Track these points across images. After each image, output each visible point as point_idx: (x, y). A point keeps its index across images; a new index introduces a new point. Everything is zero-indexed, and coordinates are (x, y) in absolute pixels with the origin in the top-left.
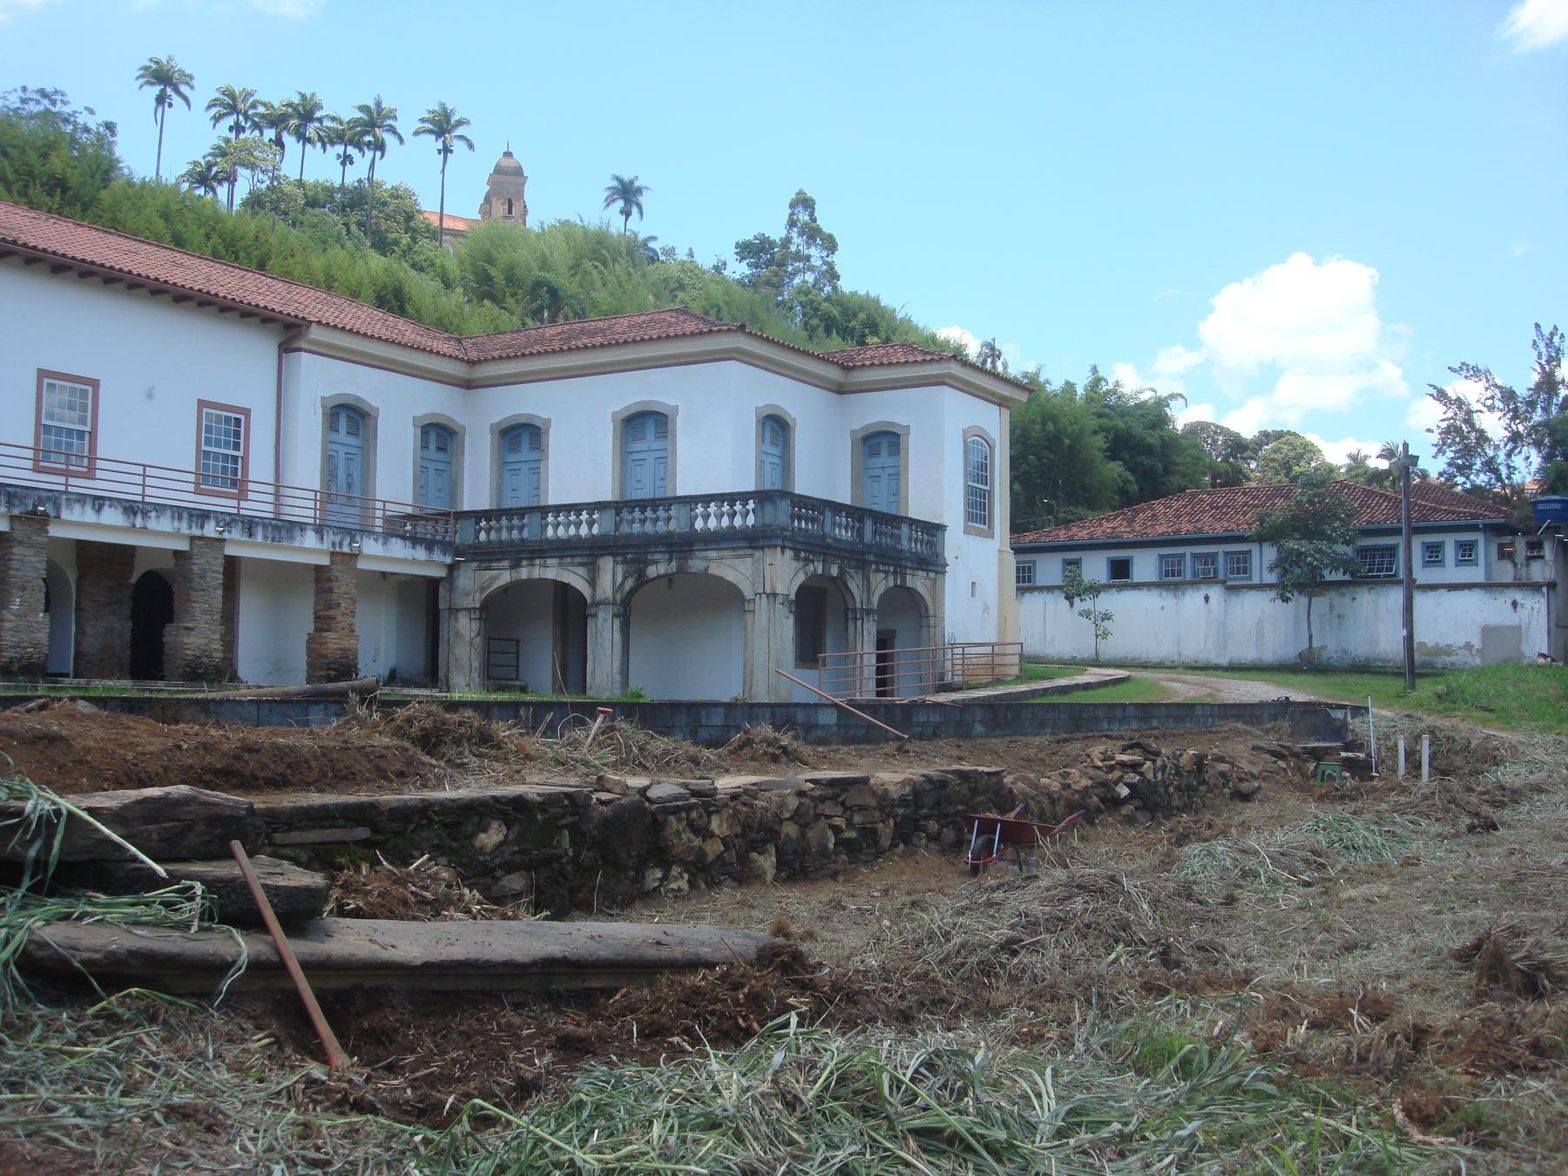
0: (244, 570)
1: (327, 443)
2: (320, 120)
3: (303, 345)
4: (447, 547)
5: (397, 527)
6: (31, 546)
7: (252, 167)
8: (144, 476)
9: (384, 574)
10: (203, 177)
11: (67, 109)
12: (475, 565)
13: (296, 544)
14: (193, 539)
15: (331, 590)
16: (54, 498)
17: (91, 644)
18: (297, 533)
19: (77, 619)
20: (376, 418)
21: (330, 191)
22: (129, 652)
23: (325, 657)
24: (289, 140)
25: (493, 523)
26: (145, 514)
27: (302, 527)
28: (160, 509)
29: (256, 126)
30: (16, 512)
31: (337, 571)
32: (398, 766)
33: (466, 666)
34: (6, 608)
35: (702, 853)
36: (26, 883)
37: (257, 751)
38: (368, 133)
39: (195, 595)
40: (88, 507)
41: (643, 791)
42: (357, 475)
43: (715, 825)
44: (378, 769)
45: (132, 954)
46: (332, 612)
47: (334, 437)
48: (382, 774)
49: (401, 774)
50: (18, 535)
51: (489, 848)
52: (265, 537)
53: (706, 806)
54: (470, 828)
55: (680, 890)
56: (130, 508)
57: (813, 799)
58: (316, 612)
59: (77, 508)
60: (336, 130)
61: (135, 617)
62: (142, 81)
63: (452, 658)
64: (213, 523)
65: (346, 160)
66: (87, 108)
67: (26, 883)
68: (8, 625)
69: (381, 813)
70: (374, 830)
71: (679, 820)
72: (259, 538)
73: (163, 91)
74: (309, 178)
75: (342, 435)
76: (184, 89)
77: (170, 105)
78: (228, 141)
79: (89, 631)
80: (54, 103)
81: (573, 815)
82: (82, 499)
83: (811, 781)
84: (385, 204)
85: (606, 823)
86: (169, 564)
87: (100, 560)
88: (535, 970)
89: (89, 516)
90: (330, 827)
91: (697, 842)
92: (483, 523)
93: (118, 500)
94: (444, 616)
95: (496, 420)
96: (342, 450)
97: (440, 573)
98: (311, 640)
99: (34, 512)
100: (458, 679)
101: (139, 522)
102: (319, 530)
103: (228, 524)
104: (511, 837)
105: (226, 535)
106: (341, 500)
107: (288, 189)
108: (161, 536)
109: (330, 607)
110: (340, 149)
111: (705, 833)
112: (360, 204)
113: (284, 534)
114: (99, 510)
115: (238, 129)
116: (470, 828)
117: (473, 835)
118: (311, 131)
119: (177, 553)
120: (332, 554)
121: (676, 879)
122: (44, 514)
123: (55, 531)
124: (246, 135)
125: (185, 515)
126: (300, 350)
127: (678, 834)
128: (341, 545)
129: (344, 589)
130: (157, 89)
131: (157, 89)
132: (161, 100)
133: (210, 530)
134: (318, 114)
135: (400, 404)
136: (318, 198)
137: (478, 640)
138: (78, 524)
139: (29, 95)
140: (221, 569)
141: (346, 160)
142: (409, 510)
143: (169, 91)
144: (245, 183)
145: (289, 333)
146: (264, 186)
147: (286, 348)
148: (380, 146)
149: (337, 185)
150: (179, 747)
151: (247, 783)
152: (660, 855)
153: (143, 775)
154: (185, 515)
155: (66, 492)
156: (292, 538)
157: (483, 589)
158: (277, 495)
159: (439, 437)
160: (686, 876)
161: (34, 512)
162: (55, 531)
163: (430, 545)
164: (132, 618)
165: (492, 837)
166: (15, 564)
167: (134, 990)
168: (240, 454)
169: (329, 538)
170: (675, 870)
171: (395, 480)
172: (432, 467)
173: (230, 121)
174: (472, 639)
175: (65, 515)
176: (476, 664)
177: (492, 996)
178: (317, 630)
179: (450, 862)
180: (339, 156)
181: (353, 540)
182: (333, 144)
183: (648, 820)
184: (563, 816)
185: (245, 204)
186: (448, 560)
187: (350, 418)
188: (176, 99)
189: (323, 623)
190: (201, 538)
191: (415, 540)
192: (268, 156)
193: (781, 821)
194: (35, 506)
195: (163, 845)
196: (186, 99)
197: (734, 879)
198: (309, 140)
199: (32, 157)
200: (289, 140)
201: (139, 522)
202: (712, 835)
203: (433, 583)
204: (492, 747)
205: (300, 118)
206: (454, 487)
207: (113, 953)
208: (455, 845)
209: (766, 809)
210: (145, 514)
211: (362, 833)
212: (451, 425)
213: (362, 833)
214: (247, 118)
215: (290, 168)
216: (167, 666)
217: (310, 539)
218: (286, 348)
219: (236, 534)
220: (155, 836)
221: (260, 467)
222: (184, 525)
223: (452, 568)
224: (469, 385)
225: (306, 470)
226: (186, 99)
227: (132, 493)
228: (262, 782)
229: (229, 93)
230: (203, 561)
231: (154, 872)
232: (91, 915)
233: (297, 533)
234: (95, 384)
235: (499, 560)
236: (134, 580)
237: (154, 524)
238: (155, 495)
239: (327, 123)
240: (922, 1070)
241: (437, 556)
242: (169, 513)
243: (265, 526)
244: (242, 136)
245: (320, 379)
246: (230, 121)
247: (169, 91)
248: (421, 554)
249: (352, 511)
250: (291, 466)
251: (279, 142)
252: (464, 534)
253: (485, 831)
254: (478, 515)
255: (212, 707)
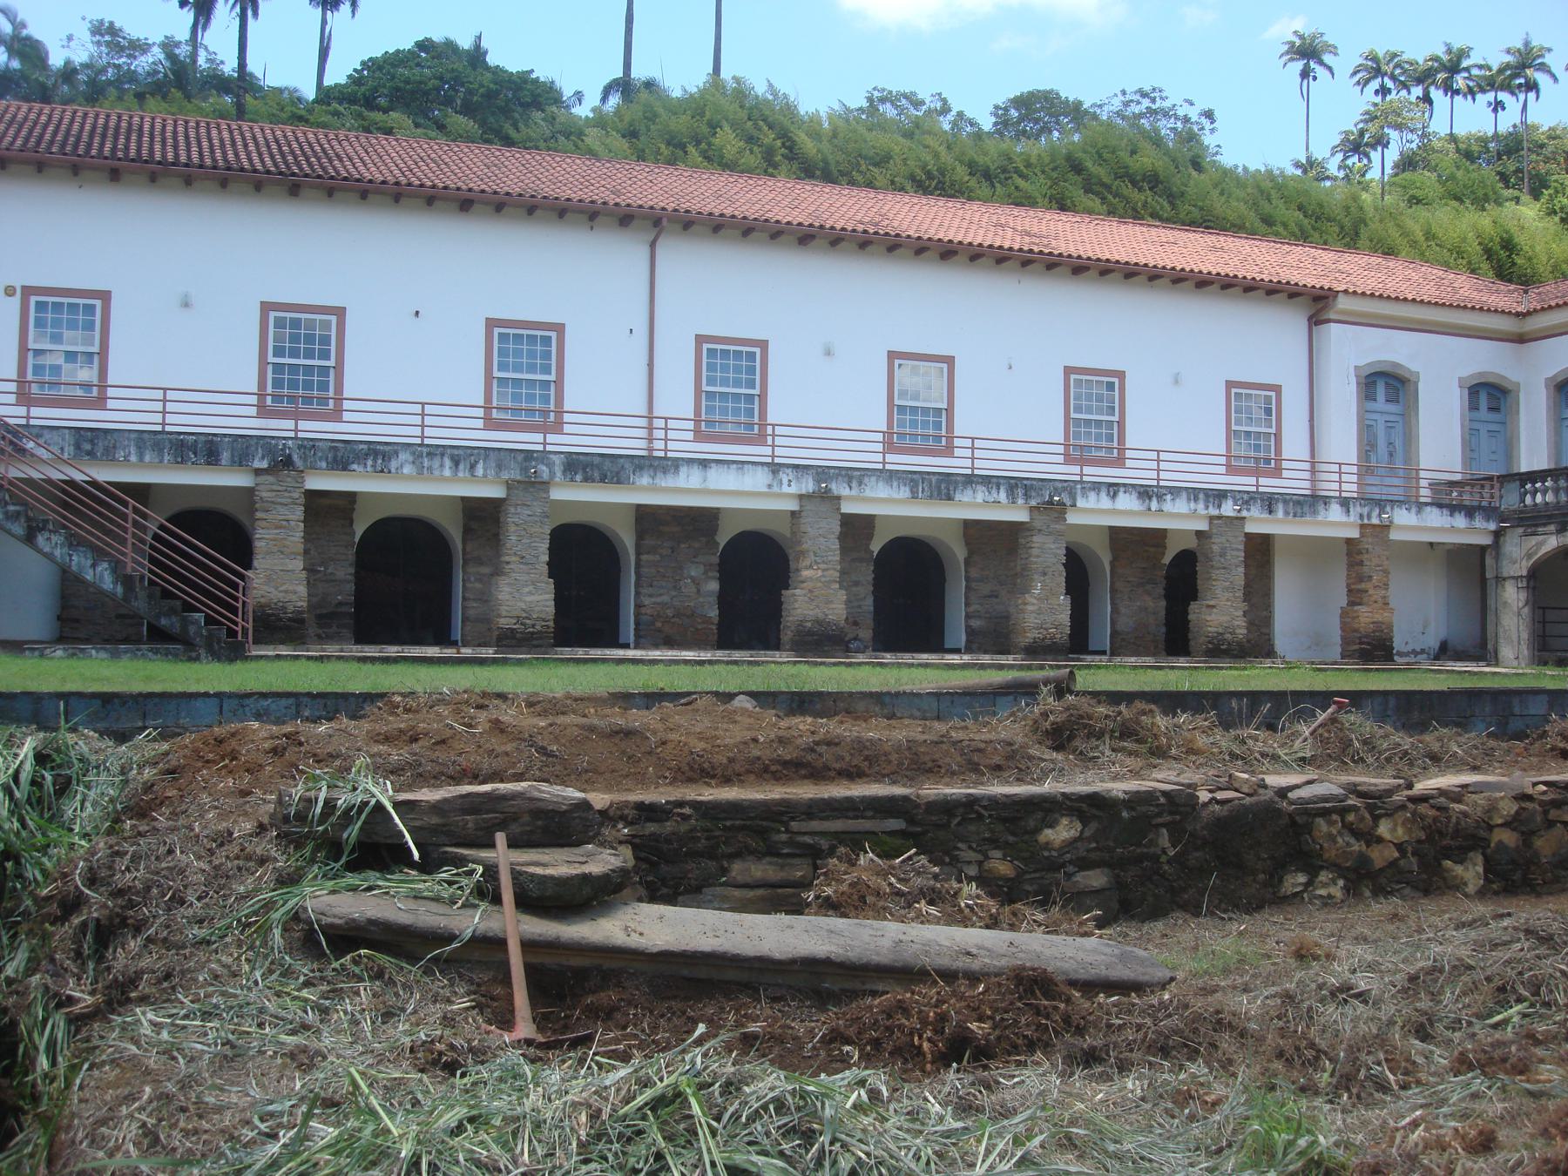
0: (1278, 548)
1: (1362, 414)
2: (1467, 69)
3: (1332, 316)
4: (1490, 512)
5: (1448, 497)
6: (1050, 533)
7: (1399, 127)
8: (1158, 461)
9: (1431, 544)
10: (1355, 145)
11: (1167, 104)
12: (1521, 530)
13: (1320, 518)
14: (1211, 518)
15: (1361, 563)
16: (1069, 487)
17: (1126, 623)
18: (1321, 507)
19: (1112, 599)
20: (1416, 384)
21: (1483, 141)
22: (1163, 630)
23: (1356, 631)
24: (1436, 94)
25: (1538, 485)
26: (1160, 498)
27: (1326, 501)
28: (1175, 491)
29: (1405, 86)
30: (1033, 503)
31: (1367, 544)
32: (997, 760)
33: (1515, 638)
34: (1028, 592)
35: (1364, 860)
36: (343, 860)
37: (837, 744)
38: (1517, 76)
39: (1215, 574)
40: (1103, 494)
41: (1282, 792)
42: (1398, 443)
43: (1384, 829)
44: (970, 762)
45: (371, 922)
46: (1363, 586)
47: (1371, 405)
48: (975, 768)
49: (998, 768)
50: (1037, 524)
51: (1057, 844)
52: (1286, 513)
53: (1371, 808)
54: (1032, 823)
55: (1330, 896)
56: (1145, 493)
57: (1542, 804)
58: (1348, 585)
59: (1092, 495)
60: (1484, 77)
61: (1168, 596)
62: (1286, 58)
63: (1501, 630)
64: (1230, 502)
65: (1498, 106)
66: (1186, 101)
67: (343, 860)
68: (1030, 608)
69: (918, 806)
70: (911, 821)
71: (1331, 823)
72: (1280, 514)
73: (1307, 66)
74: (1461, 131)
75: (1381, 403)
76: (1327, 58)
77: (1315, 78)
78: (1375, 105)
79: (1123, 610)
80: (1153, 101)
81: (1171, 813)
82: (1096, 487)
83: (1545, 783)
84: (1542, 146)
85: (1220, 824)
86: (1192, 544)
87: (1133, 545)
88: (796, 967)
89: (1105, 502)
90: (856, 818)
91: (1357, 846)
92: (1528, 486)
93: (1133, 486)
94: (1491, 584)
95: (1551, 374)
96: (1381, 419)
97: (1486, 540)
98: (1344, 614)
99: (1051, 502)
100: (1506, 652)
101: (1154, 505)
102: (1345, 503)
103: (1247, 502)
104: (1087, 834)
105: (1244, 513)
106: (1381, 472)
107: (1436, 144)
108: (1180, 519)
109: (1361, 579)
110: (1490, 96)
111: (1372, 839)
112: (1518, 150)
113: (1306, 509)
114: (1114, 497)
115: (1383, 91)
116: (1032, 823)
117: (1038, 830)
118: (1460, 81)
119: (1199, 533)
120: (1362, 526)
121: (1325, 885)
122: (1061, 503)
123: (1072, 518)
124: (1392, 96)
125: (1201, 496)
126: (1329, 321)
127: (1332, 838)
128: (1369, 517)
129: (1375, 561)
130: (1300, 65)
131: (1300, 65)
132: (1305, 74)
133: (1228, 509)
134: (1465, 64)
135: (1442, 369)
136: (1468, 151)
137: (1526, 610)
138: (1094, 513)
139: (1128, 97)
140: (1242, 547)
141: (1498, 106)
142: (1458, 477)
143: (1312, 64)
144: (1398, 145)
145: (1317, 305)
146: (1414, 146)
147: (1316, 321)
148: (1532, 86)
149: (1490, 134)
150: (755, 740)
151: (817, 774)
152: (1311, 862)
153: (706, 765)
154: (1201, 496)
155: (1081, 482)
156: (1315, 513)
157: (1529, 556)
158: (1313, 471)
159: (1489, 397)
160: (1341, 883)
161: (1051, 502)
162: (1072, 518)
163: (1470, 512)
164: (1167, 597)
165: (1062, 832)
166: (1035, 552)
167: (362, 952)
168: (332, 363)
169: (1356, 510)
170: (1324, 876)
171: (1440, 445)
172: (1484, 428)
173: (1375, 84)
174: (1519, 610)
175: (1081, 503)
176: (1525, 635)
177: (751, 989)
178: (1351, 603)
179: (1005, 856)
180: (1490, 104)
181: (1382, 511)
182: (1483, 91)
183: (1286, 820)
184: (1159, 815)
185: (1396, 166)
186: (1492, 526)
187: (1387, 386)
188: (1320, 71)
189: (1355, 597)
190: (1220, 517)
191: (1453, 509)
192: (1415, 116)
193: (1491, 828)
194: (1051, 497)
195: (480, 833)
196: (1330, 69)
197: (1416, 888)
198: (1457, 92)
199: (1124, 155)
200: (1436, 94)
201: (1154, 505)
202: (1380, 840)
203: (1483, 549)
204: (1137, 741)
205: (1447, 72)
206: (1509, 449)
207: (354, 920)
208: (1011, 839)
209: (1465, 815)
210: (1160, 498)
211: (895, 824)
212: (1504, 384)
213: (895, 824)
214: (1393, 78)
215: (1439, 125)
216: (1192, 643)
217: (1335, 513)
218: (1316, 321)
219: (1255, 512)
220: (470, 825)
221: (1294, 445)
222: (1201, 506)
223: (1498, 534)
224: (1521, 339)
225: (1342, 444)
226: (1330, 69)
227: (1147, 477)
228: (832, 774)
229: (1373, 58)
230: (1223, 539)
231: (411, 854)
232: (379, 887)
233: (1321, 507)
234: (1121, 375)
235: (1545, 525)
236: (1167, 560)
237: (1168, 506)
238: (1169, 478)
239: (1475, 72)
240: (771, 1107)
241: (1479, 522)
242: (1184, 495)
243: (1285, 502)
244: (1388, 98)
245: (1351, 349)
246: (1375, 84)
247: (1312, 64)
248: (1460, 521)
249: (1396, 482)
250: (1326, 441)
251: (1427, 99)
252: (1510, 499)
253: (1051, 826)
254: (1533, 477)
255: (887, 699)
